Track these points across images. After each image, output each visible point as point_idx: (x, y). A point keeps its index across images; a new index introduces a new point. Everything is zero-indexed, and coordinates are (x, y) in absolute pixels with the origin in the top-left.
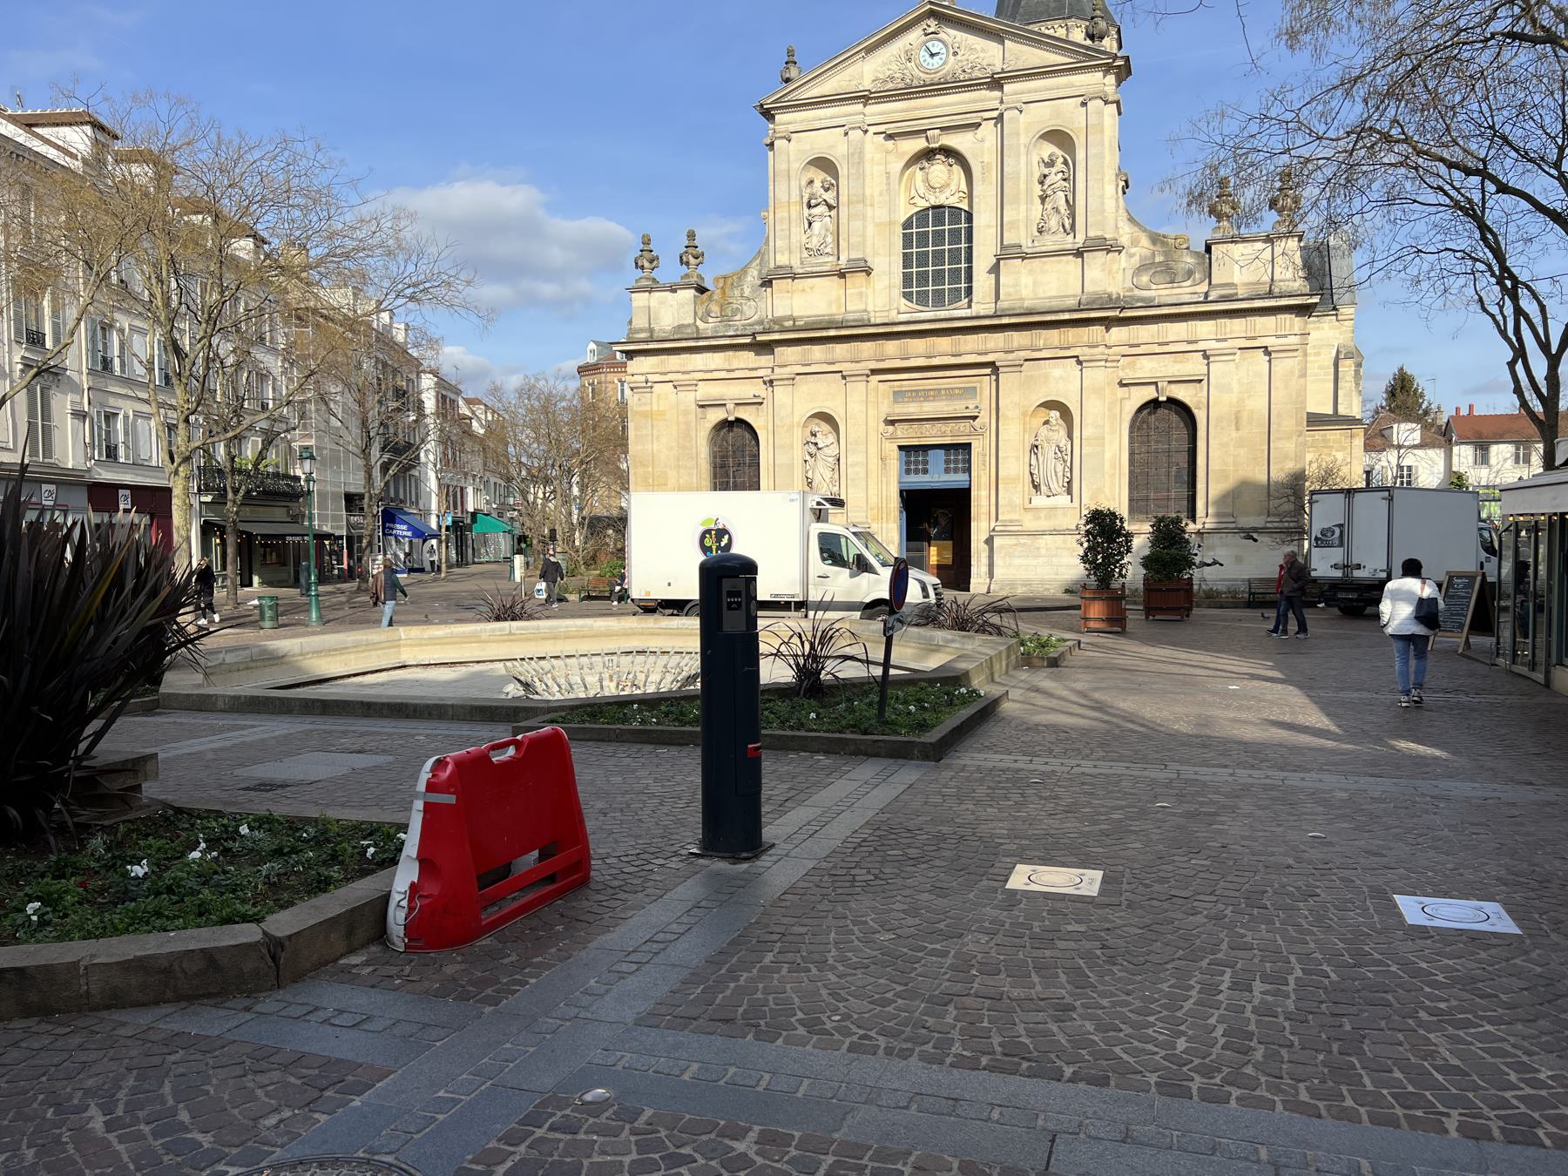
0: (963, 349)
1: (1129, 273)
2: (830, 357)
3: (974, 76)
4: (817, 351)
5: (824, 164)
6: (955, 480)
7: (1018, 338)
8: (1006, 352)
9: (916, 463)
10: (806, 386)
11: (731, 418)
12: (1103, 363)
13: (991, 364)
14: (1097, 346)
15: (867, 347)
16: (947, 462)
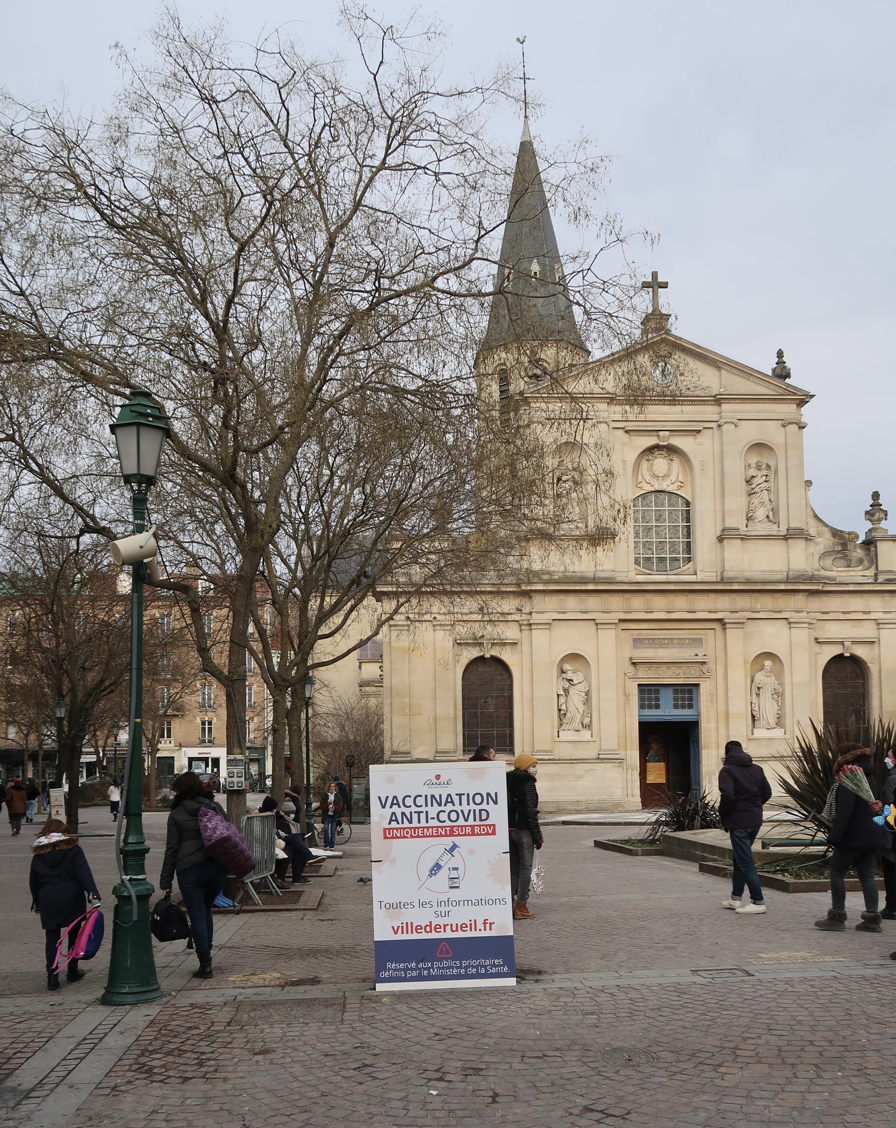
1: (817, 557)
2: (583, 607)
3: (696, 393)
4: (572, 602)
5: (760, 447)
6: (683, 714)
7: (742, 602)
9: (650, 699)
10: (560, 630)
11: (487, 656)
12: (806, 625)
13: (720, 620)
15: (616, 602)
16: (675, 699)
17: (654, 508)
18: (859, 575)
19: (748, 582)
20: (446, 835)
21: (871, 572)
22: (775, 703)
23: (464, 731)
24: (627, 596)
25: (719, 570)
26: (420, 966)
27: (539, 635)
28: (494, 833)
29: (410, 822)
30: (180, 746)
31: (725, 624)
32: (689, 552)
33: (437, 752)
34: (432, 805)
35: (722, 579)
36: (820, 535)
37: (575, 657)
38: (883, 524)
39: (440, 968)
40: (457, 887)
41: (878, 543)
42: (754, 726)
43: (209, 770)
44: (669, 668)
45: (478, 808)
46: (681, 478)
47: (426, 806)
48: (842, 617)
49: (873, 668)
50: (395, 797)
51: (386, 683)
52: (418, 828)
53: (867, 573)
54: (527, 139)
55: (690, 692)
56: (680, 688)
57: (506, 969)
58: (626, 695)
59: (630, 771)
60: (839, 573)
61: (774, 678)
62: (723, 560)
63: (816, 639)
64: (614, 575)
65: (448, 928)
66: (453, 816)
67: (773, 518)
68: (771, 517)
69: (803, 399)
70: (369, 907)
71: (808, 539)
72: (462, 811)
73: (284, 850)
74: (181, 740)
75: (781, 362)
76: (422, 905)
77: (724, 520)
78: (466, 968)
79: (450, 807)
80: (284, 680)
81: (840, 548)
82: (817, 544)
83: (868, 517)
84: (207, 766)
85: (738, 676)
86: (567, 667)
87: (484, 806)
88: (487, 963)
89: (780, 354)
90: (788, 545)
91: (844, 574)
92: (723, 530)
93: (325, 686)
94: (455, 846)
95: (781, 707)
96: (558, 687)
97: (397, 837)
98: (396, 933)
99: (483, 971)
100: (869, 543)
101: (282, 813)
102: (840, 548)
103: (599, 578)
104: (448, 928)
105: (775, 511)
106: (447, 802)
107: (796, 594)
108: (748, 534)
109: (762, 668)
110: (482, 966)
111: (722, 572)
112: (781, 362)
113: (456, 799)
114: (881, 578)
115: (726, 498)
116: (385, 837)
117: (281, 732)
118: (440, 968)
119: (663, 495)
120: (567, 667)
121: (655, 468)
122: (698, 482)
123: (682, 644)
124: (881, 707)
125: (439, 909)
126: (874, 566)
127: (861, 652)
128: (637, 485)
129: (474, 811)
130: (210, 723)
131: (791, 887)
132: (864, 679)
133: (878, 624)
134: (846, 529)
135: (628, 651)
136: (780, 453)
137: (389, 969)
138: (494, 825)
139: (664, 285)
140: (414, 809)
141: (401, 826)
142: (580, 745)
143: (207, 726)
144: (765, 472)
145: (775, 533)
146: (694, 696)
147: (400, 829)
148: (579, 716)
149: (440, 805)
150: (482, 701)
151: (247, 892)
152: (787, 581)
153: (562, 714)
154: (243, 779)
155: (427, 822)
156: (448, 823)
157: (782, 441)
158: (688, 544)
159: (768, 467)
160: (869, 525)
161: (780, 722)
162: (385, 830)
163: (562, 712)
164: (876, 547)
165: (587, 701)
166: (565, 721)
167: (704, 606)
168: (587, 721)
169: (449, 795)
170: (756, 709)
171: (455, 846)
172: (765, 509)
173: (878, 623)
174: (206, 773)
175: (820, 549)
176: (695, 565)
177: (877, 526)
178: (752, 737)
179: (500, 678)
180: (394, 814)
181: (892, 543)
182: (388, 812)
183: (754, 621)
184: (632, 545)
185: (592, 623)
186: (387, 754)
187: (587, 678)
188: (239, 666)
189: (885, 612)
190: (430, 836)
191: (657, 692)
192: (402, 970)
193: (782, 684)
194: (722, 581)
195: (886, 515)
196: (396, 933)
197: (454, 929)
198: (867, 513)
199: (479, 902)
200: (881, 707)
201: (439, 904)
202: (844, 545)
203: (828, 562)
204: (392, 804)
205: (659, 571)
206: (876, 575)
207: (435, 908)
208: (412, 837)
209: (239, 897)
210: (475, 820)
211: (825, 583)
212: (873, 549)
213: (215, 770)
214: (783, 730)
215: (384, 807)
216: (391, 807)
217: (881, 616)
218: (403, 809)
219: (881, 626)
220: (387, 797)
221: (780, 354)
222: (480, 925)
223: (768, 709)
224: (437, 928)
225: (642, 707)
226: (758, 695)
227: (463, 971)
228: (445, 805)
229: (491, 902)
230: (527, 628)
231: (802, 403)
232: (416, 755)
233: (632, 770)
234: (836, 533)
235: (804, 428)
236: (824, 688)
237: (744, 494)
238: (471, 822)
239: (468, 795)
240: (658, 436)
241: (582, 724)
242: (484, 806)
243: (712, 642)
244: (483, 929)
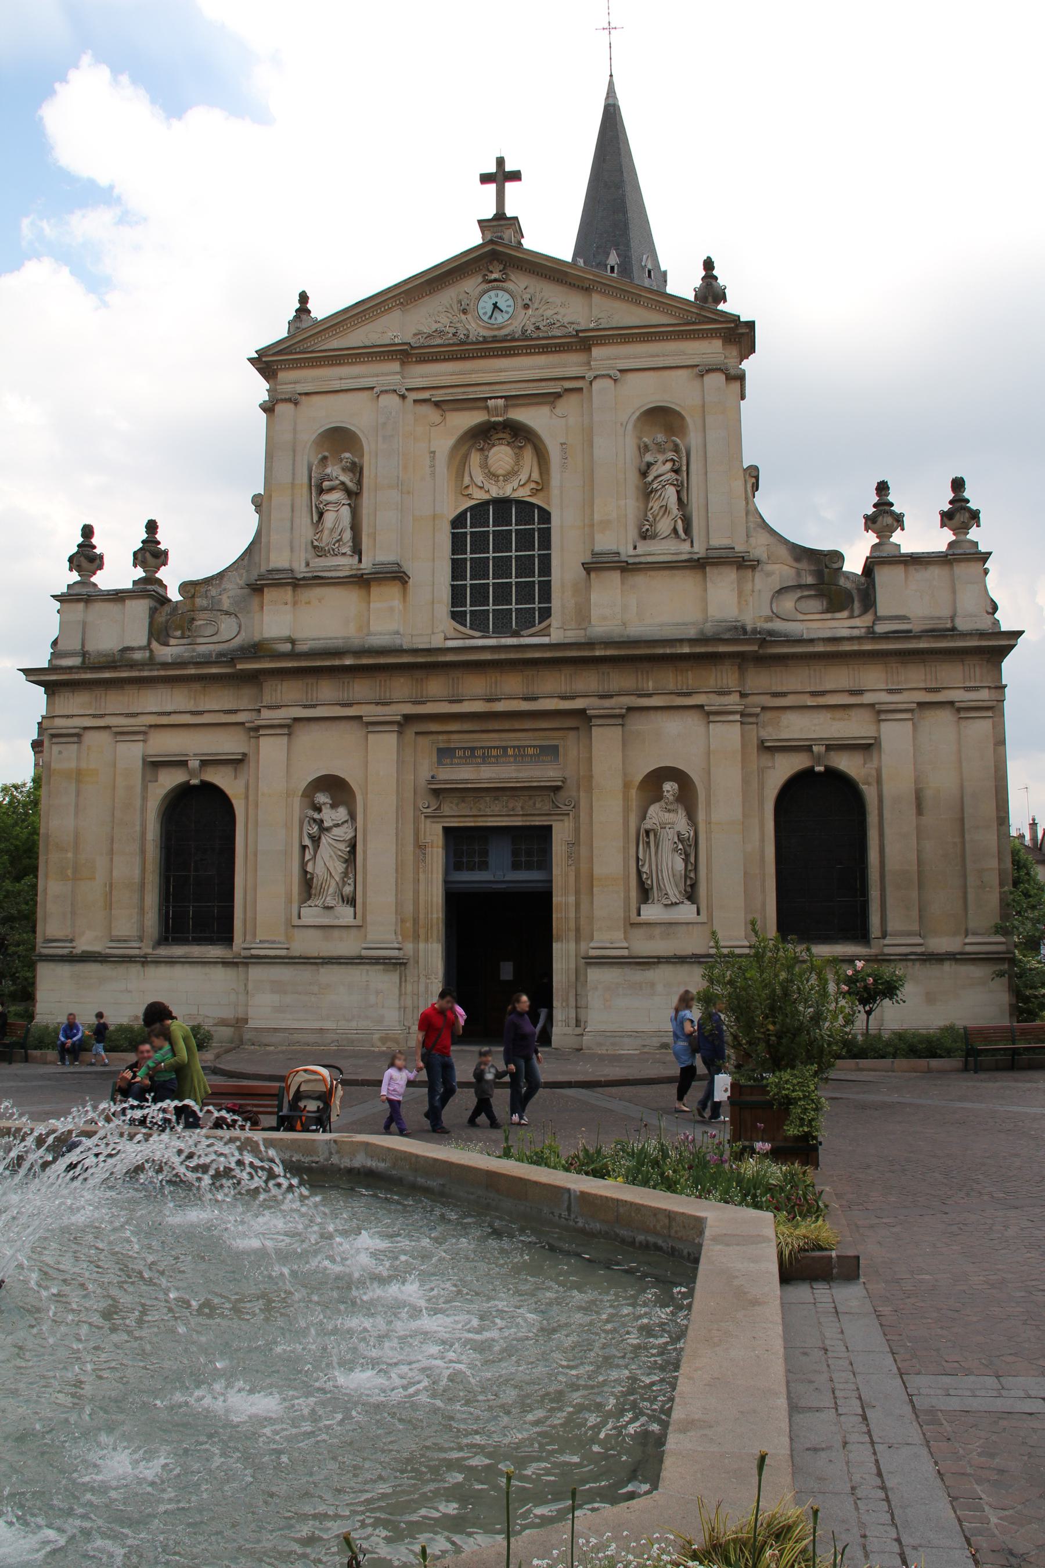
1: (767, 596)
4: (327, 690)
7: (619, 680)
8: (602, 697)
10: (307, 738)
12: (738, 717)
14: (729, 693)
15: (400, 687)
16: (515, 853)
44: (496, 798)
48: (810, 701)
49: (870, 793)
54: (611, 101)
58: (421, 847)
70: (980, 728)
109: (658, 797)
120: (322, 798)
121: (490, 462)
128: (463, 492)
133: (879, 712)
135: (426, 767)
136: (692, 422)
139: (516, 176)
142: (336, 933)
144: (670, 455)
148: (333, 884)
168: (348, 890)
170: (645, 869)
198: (867, 518)
203: (788, 604)
214: (694, 907)
221: (708, 264)
232: (83, 945)
234: (803, 554)
240: (487, 408)
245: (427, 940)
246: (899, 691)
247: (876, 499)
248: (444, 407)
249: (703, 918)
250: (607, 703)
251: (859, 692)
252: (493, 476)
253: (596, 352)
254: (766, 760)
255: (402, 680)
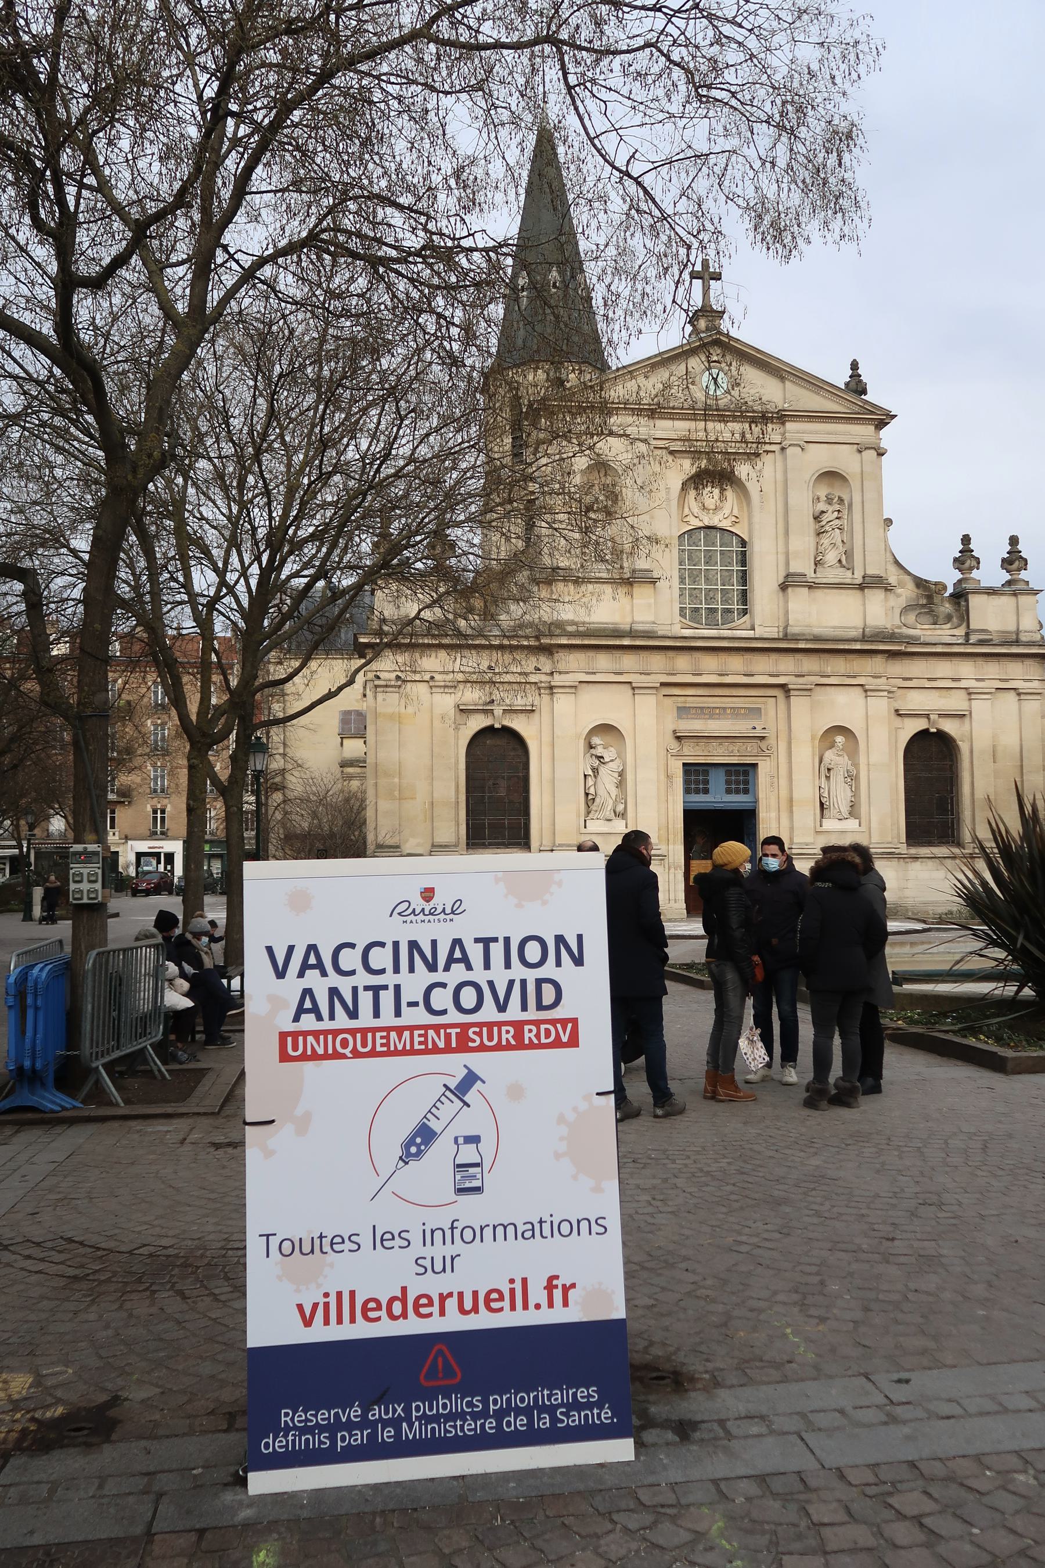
0: (829, 670)
2: (617, 667)
4: (603, 661)
5: (831, 476)
6: (738, 801)
7: (809, 664)
8: (797, 676)
9: (697, 782)
10: (588, 695)
11: (497, 726)
12: (885, 694)
13: (783, 686)
14: (880, 677)
15: (657, 661)
16: (728, 782)
17: (703, 548)
18: (947, 634)
19: (817, 639)
20: (448, 1049)
21: (961, 631)
22: (848, 788)
23: (467, 820)
24: (671, 654)
25: (782, 625)
26: (375, 1414)
27: (563, 703)
28: (574, 1042)
29: (353, 1014)
30: (127, 838)
31: (789, 690)
32: (745, 603)
33: (433, 846)
34: (412, 970)
35: (786, 635)
36: (901, 584)
37: (606, 729)
38: (975, 574)
39: (429, 1419)
40: (478, 1190)
41: (970, 597)
42: (822, 816)
43: (161, 868)
44: (721, 744)
45: (531, 976)
46: (736, 512)
47: (397, 970)
49: (964, 747)
50: (312, 948)
51: (370, 760)
52: (374, 1030)
53: (956, 632)
55: (746, 773)
56: (733, 769)
57: (606, 1414)
58: (669, 777)
59: (672, 870)
60: (924, 631)
61: (846, 758)
62: (787, 612)
63: (897, 711)
64: (656, 628)
65: (451, 1304)
66: (468, 998)
67: (846, 562)
68: (844, 562)
69: (882, 419)
71: (888, 589)
72: (491, 983)
73: (187, 995)
74: (128, 831)
75: (855, 375)
76: (382, 1240)
77: (787, 564)
78: (500, 1415)
79: (458, 973)
80: (204, 735)
81: (924, 602)
82: (899, 596)
83: (957, 565)
84: (159, 862)
85: (804, 754)
86: (596, 740)
87: (548, 970)
88: (558, 1397)
89: (854, 366)
90: (864, 597)
91: (929, 633)
92: (787, 576)
93: (299, 766)
94: (471, 1079)
95: (856, 793)
96: (585, 765)
97: (315, 1057)
98: (308, 1323)
99: (545, 1422)
100: (960, 596)
101: (189, 936)
102: (924, 602)
103: (636, 631)
104: (451, 1304)
105: (849, 554)
106: (450, 960)
107: (873, 655)
108: (817, 581)
110: (544, 1408)
111: (786, 627)
112: (855, 375)
113: (475, 953)
114: (973, 639)
115: (791, 537)
116: (284, 1057)
117: (199, 812)
118: (429, 1419)
119: (714, 531)
120: (596, 740)
122: (757, 517)
123: (737, 715)
124: (973, 794)
125: (428, 1251)
126: (965, 624)
127: (949, 727)
128: (683, 519)
129: (523, 982)
130: (163, 812)
131: (1010, 1066)
132: (952, 760)
134: (933, 578)
135: (671, 722)
136: (855, 484)
137: (287, 1429)
138: (575, 1021)
139: (717, 277)
140: (363, 979)
141: (326, 1025)
143: (159, 815)
144: (837, 507)
145: (848, 581)
146: (750, 778)
147: (326, 1033)
148: (611, 802)
149: (432, 967)
150: (491, 782)
151: (98, 1082)
152: (864, 639)
153: (589, 799)
154: (98, 886)
155: (398, 1013)
156: (454, 1017)
157: (858, 470)
158: (744, 593)
159: (841, 500)
160: (958, 575)
161: (854, 811)
162: (283, 1036)
163: (590, 797)
164: (967, 601)
165: (621, 784)
166: (594, 808)
167: (763, 669)
168: (620, 808)
169: (457, 942)
170: (826, 795)
171: (471, 1079)
172: (837, 552)
173: (969, 693)
174: (157, 871)
175: (902, 602)
176: (752, 618)
177: (968, 576)
178: (819, 829)
179: (512, 754)
180: (308, 992)
181: (986, 596)
182: (292, 987)
183: (823, 688)
184: (676, 593)
185: (627, 687)
186: (371, 847)
187: (621, 755)
188: (94, 694)
189: (977, 680)
190: (404, 1052)
191: (706, 773)
192: (322, 1429)
193: (856, 765)
194: (786, 638)
195: (979, 563)
196: (308, 1323)
197: (468, 1305)
199: (533, 1230)
200: (973, 794)
201: (428, 1236)
202: (930, 598)
203: (911, 618)
204: (305, 967)
205: (712, 624)
206: (967, 635)
207: (417, 1248)
208: (356, 1054)
209: (86, 1090)
210: (524, 1008)
211: (908, 643)
212: (963, 603)
213: (169, 868)
215: (281, 974)
216: (301, 975)
217: (972, 684)
218: (334, 980)
219: (973, 697)
220: (291, 949)
221: (854, 366)
222: (537, 1294)
223: (840, 795)
224: (421, 1305)
225: (687, 791)
226: (828, 778)
227: (490, 1424)
228: (447, 968)
229: (565, 1228)
230: (547, 691)
231: (881, 424)
233: (676, 869)
234: (920, 583)
235: (883, 455)
236: (905, 770)
237: (812, 533)
238: (514, 1012)
239: (507, 940)
241: (615, 812)
242: (548, 970)
243: (772, 713)
244: (544, 1303)
245: (674, 844)
246: (982, 680)
247: (961, 547)
248: (677, 455)
249: (863, 828)
250: (801, 680)
251: (959, 680)
252: (704, 508)
253: (789, 426)
254: (898, 721)
255: (658, 657)
